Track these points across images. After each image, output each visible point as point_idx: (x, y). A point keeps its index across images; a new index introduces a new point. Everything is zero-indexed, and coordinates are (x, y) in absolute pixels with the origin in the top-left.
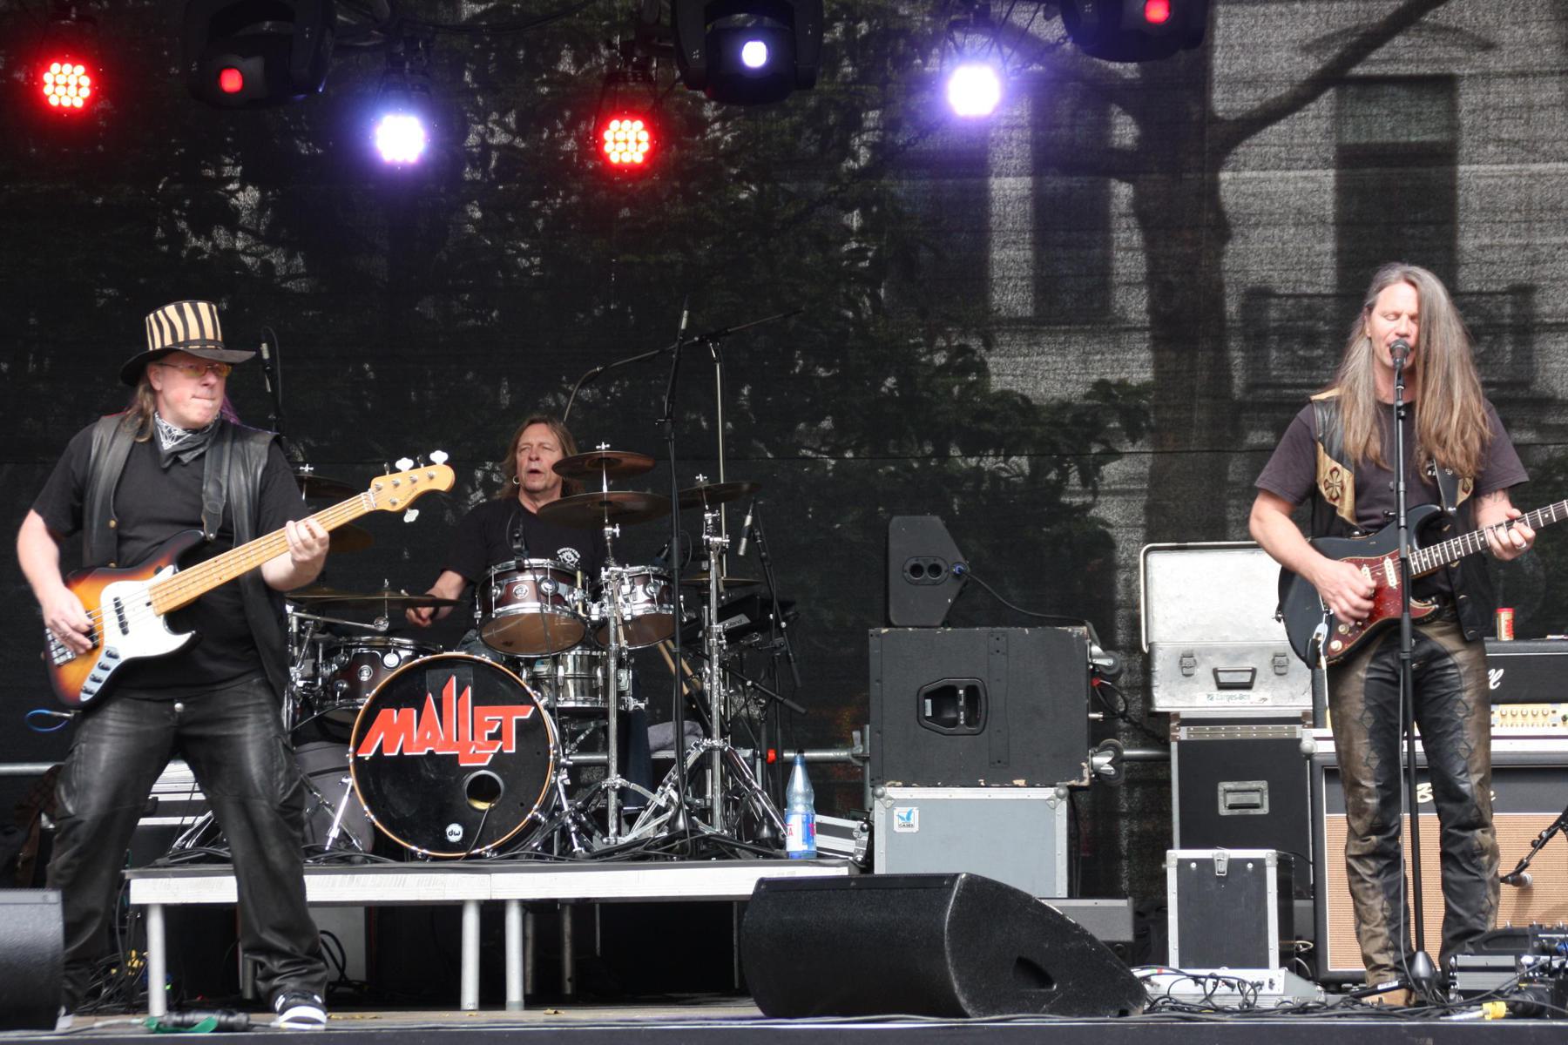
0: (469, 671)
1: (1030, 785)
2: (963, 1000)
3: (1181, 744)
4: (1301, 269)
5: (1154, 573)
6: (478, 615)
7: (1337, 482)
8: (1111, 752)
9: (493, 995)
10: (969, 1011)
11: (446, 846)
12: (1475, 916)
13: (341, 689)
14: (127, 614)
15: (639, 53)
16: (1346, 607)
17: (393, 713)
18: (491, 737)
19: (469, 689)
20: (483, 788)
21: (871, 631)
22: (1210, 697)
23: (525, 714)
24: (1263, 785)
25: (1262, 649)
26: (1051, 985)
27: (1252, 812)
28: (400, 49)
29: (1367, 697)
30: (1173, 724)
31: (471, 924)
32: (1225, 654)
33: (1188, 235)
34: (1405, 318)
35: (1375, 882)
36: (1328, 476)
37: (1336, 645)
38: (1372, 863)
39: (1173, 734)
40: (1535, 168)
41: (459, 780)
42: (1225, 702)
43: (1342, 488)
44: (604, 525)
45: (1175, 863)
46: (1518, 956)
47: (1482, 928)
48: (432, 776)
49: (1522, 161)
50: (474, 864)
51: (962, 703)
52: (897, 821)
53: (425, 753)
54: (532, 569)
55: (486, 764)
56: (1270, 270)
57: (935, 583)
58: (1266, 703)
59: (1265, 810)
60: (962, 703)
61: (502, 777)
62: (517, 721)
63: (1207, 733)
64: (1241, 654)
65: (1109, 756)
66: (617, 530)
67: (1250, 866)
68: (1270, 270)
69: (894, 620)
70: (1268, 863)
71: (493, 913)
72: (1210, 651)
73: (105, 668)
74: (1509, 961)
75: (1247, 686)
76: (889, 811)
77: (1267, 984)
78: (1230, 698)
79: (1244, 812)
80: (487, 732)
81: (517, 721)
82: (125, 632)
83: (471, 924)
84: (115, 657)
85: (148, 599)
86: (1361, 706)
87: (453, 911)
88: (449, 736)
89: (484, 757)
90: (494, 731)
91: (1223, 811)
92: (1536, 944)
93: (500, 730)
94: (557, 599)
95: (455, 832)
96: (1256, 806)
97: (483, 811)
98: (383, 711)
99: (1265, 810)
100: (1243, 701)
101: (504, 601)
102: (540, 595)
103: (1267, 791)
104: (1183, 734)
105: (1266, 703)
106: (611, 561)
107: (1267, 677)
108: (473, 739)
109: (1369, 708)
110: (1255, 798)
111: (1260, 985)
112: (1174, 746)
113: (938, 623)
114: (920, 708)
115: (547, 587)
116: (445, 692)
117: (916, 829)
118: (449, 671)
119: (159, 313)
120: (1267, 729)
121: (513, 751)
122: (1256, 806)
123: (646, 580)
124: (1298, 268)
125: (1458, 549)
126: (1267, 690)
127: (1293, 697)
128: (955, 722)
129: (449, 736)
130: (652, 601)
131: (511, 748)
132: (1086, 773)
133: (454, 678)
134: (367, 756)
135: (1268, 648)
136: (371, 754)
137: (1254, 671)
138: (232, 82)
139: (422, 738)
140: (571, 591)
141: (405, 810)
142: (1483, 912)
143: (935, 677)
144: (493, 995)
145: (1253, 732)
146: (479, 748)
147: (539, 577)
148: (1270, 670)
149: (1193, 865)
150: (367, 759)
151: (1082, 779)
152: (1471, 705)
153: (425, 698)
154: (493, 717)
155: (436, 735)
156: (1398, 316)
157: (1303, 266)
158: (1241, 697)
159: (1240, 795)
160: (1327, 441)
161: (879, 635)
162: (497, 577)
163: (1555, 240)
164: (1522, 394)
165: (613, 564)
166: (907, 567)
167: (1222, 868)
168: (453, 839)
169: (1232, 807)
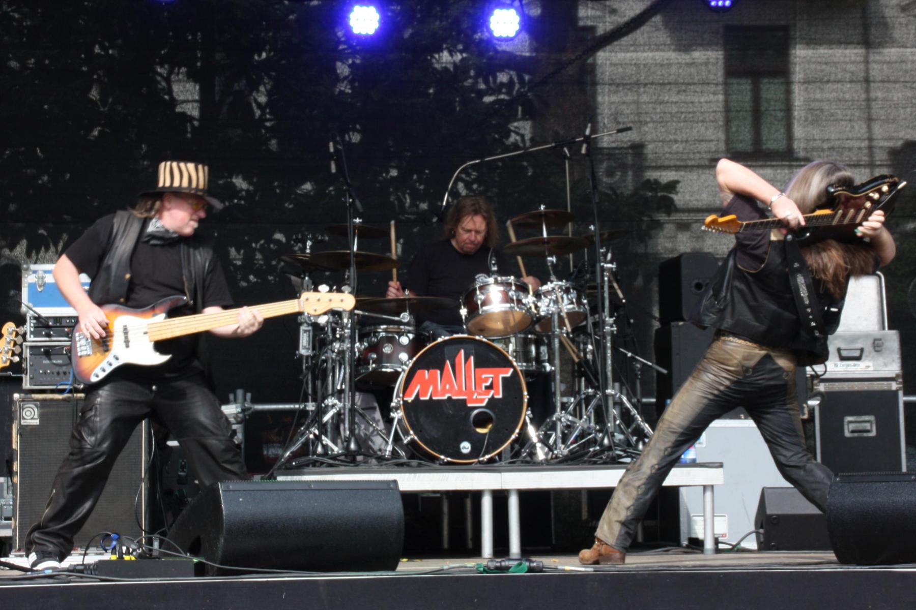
4: (854, 109)
6: (463, 312)
8: (819, 398)
13: (373, 359)
14: (130, 336)
17: (437, 374)
18: (487, 388)
20: (482, 421)
21: (673, 324)
22: (836, 365)
23: (507, 373)
24: (872, 418)
25: (866, 336)
27: (865, 435)
39: (901, 386)
42: (844, 368)
48: (451, 412)
50: (490, 466)
53: (445, 398)
55: (484, 404)
56: (836, 109)
58: (869, 369)
61: (494, 412)
63: (837, 387)
65: (818, 400)
68: (836, 109)
69: (685, 316)
70: (238, 431)
71: (500, 498)
73: (110, 365)
75: (858, 358)
78: (848, 365)
80: (484, 385)
82: (127, 346)
84: (117, 359)
85: (146, 330)
87: (477, 495)
89: (482, 401)
90: (488, 384)
93: (492, 384)
94: (519, 301)
96: (868, 431)
99: (873, 433)
100: (856, 367)
101: (484, 303)
102: (507, 299)
103: (874, 422)
105: (869, 369)
106: (553, 278)
107: (870, 353)
108: (475, 388)
110: (867, 426)
118: (459, 346)
119: (176, 184)
120: (874, 384)
121: (500, 396)
122: (868, 431)
124: (852, 107)
126: (870, 361)
127: (886, 365)
129: (460, 387)
131: (499, 394)
133: (462, 352)
137: (862, 350)
139: (444, 388)
140: (526, 297)
141: (435, 433)
145: (857, 386)
146: (479, 394)
148: (871, 349)
150: (410, 401)
153: (444, 363)
154: (488, 375)
157: (855, 107)
158: (855, 365)
159: (858, 425)
161: (678, 326)
165: (555, 280)
169: (853, 432)
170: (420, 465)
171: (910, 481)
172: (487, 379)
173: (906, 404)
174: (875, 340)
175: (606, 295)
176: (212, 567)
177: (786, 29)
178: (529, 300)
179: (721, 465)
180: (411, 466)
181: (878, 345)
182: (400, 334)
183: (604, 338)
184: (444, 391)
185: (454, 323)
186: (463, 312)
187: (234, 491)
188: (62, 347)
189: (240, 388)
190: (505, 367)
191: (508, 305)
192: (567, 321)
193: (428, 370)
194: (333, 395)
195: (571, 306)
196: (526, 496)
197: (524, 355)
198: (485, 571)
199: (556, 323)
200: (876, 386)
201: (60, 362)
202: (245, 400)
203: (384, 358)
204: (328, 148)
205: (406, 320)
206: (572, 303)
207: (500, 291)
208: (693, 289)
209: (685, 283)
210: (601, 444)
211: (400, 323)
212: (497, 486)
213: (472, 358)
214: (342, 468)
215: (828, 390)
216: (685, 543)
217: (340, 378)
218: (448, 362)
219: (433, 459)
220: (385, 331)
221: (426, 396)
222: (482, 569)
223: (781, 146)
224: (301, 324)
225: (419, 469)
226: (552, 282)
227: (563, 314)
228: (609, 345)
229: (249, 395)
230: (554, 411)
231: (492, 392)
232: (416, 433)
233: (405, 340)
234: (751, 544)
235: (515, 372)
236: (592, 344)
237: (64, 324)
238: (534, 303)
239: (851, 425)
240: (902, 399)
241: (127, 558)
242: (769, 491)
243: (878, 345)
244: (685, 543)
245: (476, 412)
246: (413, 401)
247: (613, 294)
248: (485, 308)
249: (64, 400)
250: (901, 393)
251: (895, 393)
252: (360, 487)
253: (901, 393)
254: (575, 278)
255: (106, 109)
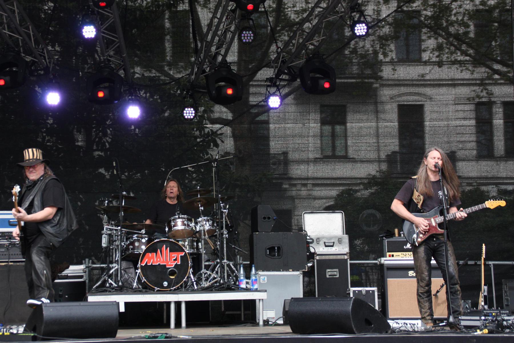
0: (168, 244)
1: (293, 271)
2: (355, 330)
3: (317, 260)
5: (305, 219)
6: (167, 229)
7: (418, 197)
9: (178, 325)
10: (356, 332)
11: (163, 287)
12: (457, 307)
15: (191, 92)
16: (422, 229)
18: (174, 260)
19: (168, 248)
20: (172, 273)
22: (323, 249)
24: (337, 270)
26: (372, 325)
27: (335, 277)
28: (132, 90)
29: (425, 252)
30: (315, 255)
31: (173, 307)
32: (327, 238)
33: (306, 139)
34: (437, 158)
35: (427, 299)
36: (417, 197)
37: (419, 240)
38: (425, 294)
40: (385, 124)
41: (167, 271)
42: (327, 250)
43: (420, 200)
44: (199, 207)
45: (352, 291)
46: (480, 317)
47: (458, 310)
49: (382, 123)
51: (276, 251)
52: (261, 280)
53: (158, 264)
54: (182, 218)
55: (173, 267)
57: (269, 221)
59: (338, 276)
60: (276, 251)
61: (177, 270)
62: (181, 256)
63: (324, 257)
64: (331, 238)
66: (203, 208)
67: (371, 292)
69: (259, 230)
71: (178, 304)
72: (323, 238)
74: (478, 318)
75: (332, 246)
76: (259, 277)
77: (416, 324)
79: (333, 277)
80: (173, 259)
81: (181, 256)
83: (173, 307)
86: (423, 254)
87: (168, 303)
88: (164, 260)
89: (172, 265)
90: (175, 258)
91: (328, 276)
92: (483, 314)
93: (176, 258)
94: (188, 225)
95: (165, 284)
96: (336, 275)
97: (173, 279)
98: (147, 254)
99: (338, 276)
101: (174, 226)
102: (184, 224)
104: (318, 258)
106: (202, 216)
107: (337, 244)
109: (425, 254)
110: (335, 273)
111: (415, 324)
112: (315, 261)
113: (270, 231)
114: (266, 252)
115: (186, 222)
116: (162, 249)
117: (266, 282)
121: (180, 263)
122: (336, 275)
123: (208, 221)
125: (451, 216)
127: (343, 249)
128: (275, 255)
129: (164, 260)
130: (210, 226)
132: (307, 268)
133: (165, 245)
134: (143, 265)
135: (337, 237)
136: (144, 264)
137: (334, 243)
138: (101, 94)
140: (191, 223)
141: (153, 278)
142: (459, 306)
143: (269, 245)
144: (178, 325)
145: (331, 257)
146: (171, 263)
147: (184, 220)
148: (338, 242)
149: (357, 292)
151: (306, 269)
152: (451, 254)
154: (175, 255)
155: (160, 259)
156: (435, 158)
159: (332, 273)
160: (417, 188)
161: (256, 234)
162: (173, 220)
163: (390, 141)
164: (286, 177)
166: (262, 217)
167: (364, 292)
168: (165, 286)
169: (330, 275)
170: (146, 292)
171: (319, 301)
172: (174, 256)
173: (350, 264)
174: (339, 239)
175: (224, 222)
176: (40, 337)
177: (344, 107)
178: (192, 224)
179: (266, 291)
180: (143, 292)
181: (340, 241)
182: (142, 238)
183: (223, 239)
184: (157, 261)
185: (164, 233)
186: (167, 229)
187: (48, 306)
188: (4, 244)
189: (87, 258)
190: (181, 252)
191: (184, 227)
192: (206, 233)
193: (151, 253)
194: (115, 263)
195: (210, 227)
196: (188, 303)
197: (191, 247)
198: (148, 338)
199: (203, 234)
200: (339, 257)
201: (3, 250)
202: (89, 263)
203: (136, 248)
204: (113, 164)
205: (144, 233)
206: (210, 226)
207: (181, 221)
208: (262, 219)
209: (259, 216)
210: (219, 283)
211: (142, 234)
212: (176, 300)
213: (168, 248)
214: (115, 293)
215: (320, 259)
216: (261, 323)
217: (118, 256)
218: (159, 250)
219: (153, 290)
220: (137, 237)
221: (150, 263)
222: (147, 337)
223: (342, 153)
224: (103, 234)
225: (146, 293)
226: (201, 217)
227: (206, 231)
228: (225, 242)
229: (91, 261)
230: (202, 269)
231: (176, 262)
232: (145, 279)
233: (144, 241)
234: (281, 322)
235: (186, 254)
236: (219, 242)
237: (6, 235)
238: (194, 226)
239: (329, 273)
240: (349, 262)
241: (6, 334)
242: (287, 301)
243: (340, 241)
244: (261, 323)
245: (170, 269)
246: (145, 265)
247: (226, 222)
248: (174, 228)
249: (5, 265)
250: (348, 260)
251: (347, 259)
252: (101, 304)
253: (348, 260)
254: (212, 215)
255: (471, 23)
